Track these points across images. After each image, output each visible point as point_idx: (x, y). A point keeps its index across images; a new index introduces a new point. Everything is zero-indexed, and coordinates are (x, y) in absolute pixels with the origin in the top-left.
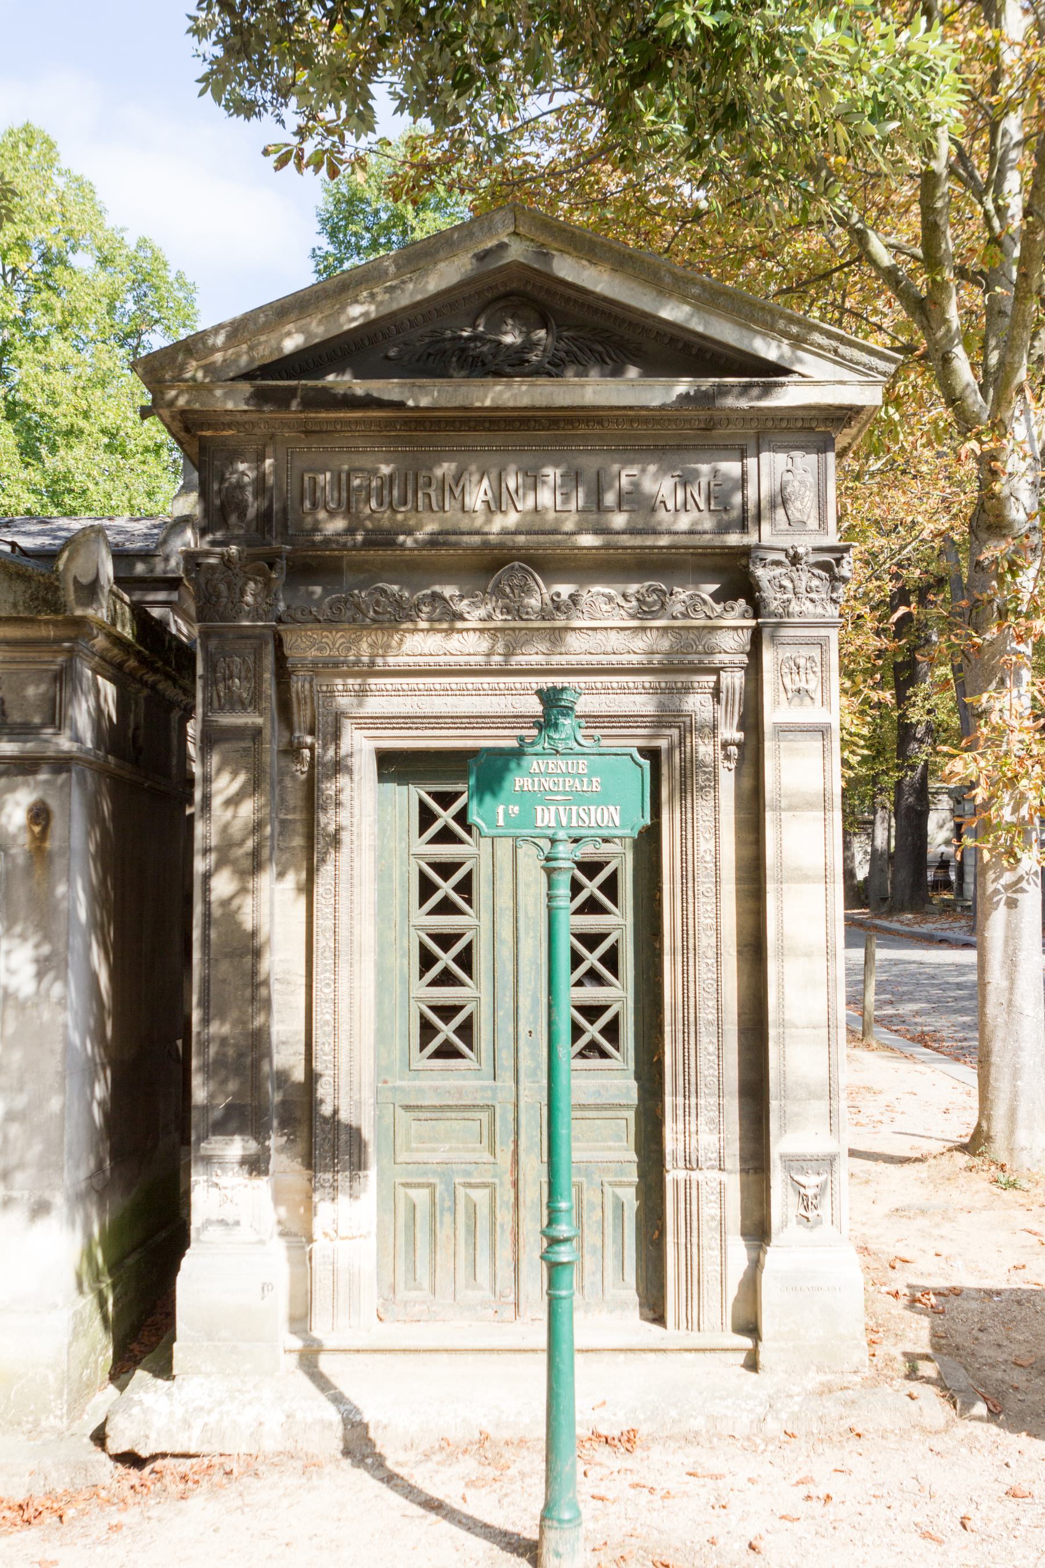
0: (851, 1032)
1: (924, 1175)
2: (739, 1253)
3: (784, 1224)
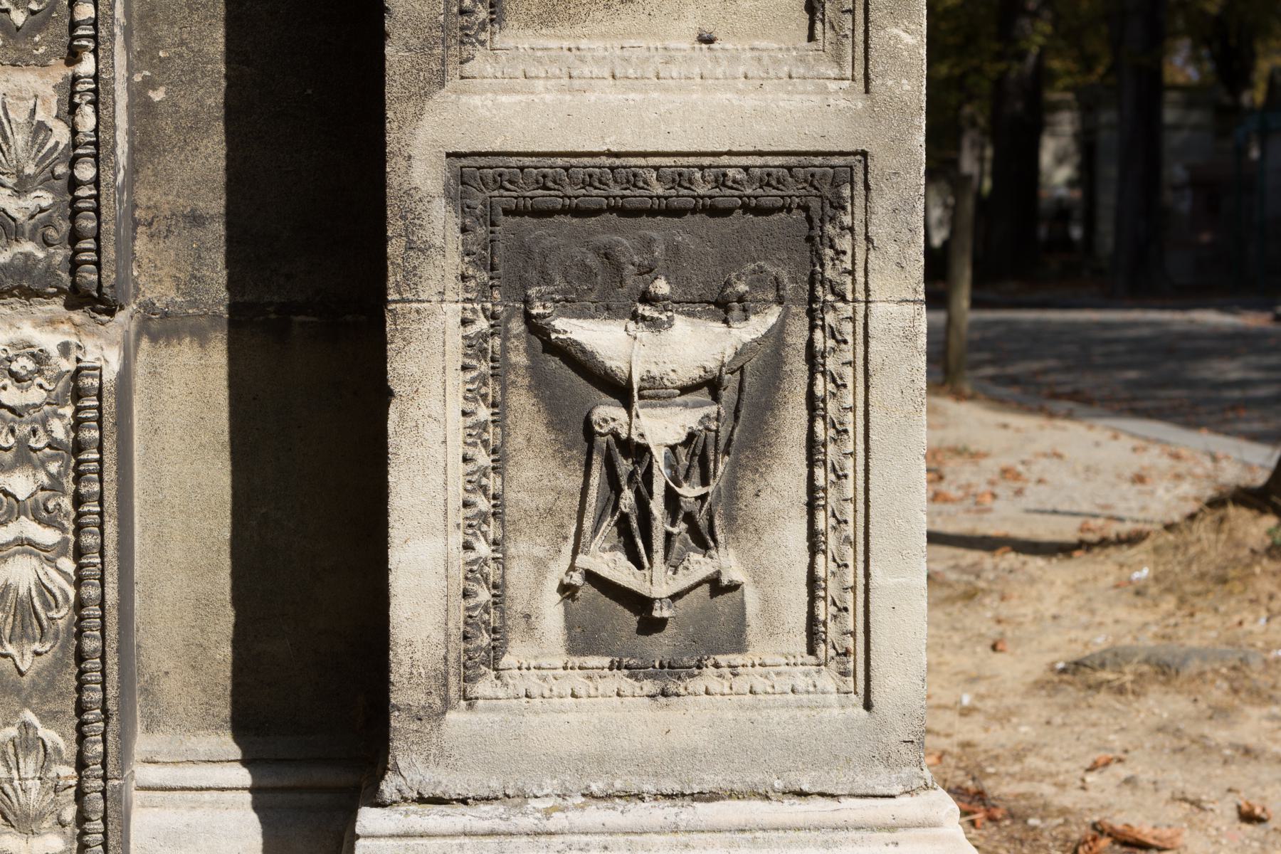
0: (944, 426)
3: (483, 641)
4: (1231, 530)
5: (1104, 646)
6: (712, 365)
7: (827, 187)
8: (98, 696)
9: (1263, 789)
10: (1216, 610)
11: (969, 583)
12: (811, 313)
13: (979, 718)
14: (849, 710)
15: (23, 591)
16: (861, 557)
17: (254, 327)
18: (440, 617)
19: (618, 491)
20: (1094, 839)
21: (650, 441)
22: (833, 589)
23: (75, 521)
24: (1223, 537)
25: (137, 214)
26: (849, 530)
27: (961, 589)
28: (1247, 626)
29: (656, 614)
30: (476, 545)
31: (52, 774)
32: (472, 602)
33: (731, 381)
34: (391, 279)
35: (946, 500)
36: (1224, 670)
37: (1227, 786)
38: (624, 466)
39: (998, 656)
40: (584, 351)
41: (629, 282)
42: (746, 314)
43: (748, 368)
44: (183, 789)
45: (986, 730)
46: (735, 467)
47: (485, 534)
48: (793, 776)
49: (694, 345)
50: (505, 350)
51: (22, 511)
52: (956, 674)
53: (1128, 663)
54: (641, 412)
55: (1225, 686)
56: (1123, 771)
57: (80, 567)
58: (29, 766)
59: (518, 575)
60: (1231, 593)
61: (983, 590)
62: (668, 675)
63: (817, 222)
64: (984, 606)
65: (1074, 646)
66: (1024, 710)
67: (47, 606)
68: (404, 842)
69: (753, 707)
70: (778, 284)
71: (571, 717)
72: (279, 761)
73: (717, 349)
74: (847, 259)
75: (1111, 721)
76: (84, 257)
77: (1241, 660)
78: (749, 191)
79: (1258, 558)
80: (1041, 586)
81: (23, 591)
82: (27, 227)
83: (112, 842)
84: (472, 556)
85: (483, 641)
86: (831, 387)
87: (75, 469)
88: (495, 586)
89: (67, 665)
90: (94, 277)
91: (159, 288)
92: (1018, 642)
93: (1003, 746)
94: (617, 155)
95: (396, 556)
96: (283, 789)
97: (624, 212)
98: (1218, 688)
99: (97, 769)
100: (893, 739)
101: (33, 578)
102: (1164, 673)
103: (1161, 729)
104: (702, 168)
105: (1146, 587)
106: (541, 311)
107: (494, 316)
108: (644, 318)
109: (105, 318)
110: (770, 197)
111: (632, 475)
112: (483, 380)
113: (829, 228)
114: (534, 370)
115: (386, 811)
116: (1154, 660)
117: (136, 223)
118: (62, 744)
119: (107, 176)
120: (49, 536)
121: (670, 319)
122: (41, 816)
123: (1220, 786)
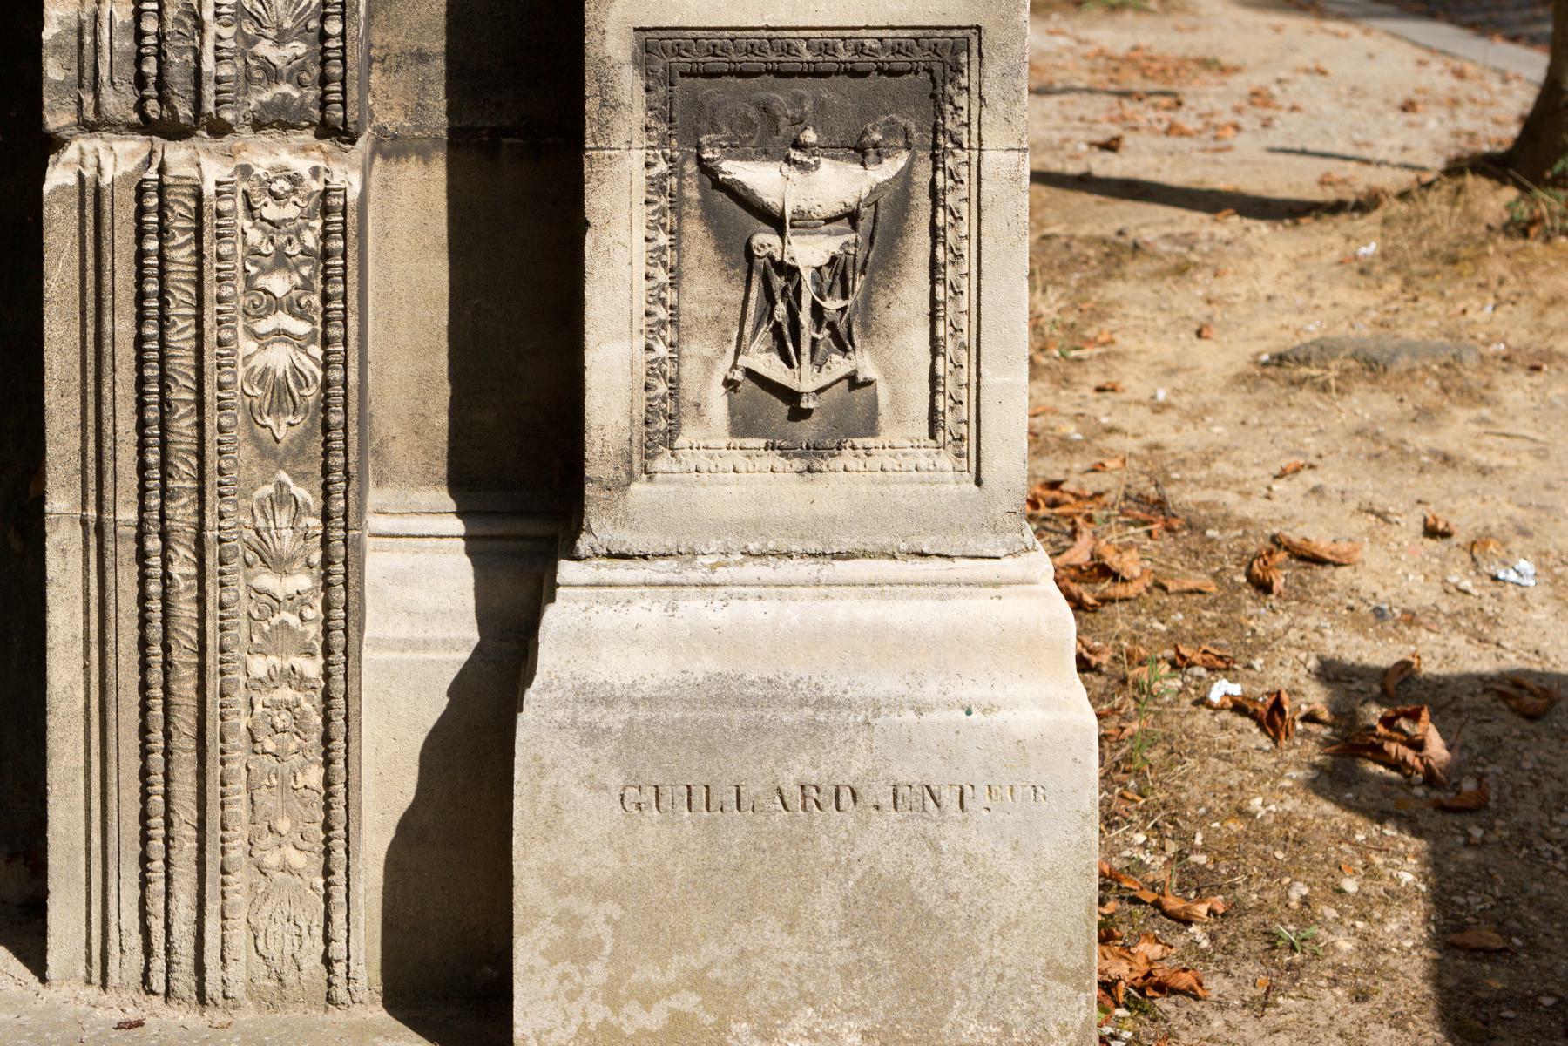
0: (1194, 29)
1: (1371, 249)
2: (422, 583)
3: (662, 426)
4: (1467, 202)
5: (1317, 336)
6: (851, 201)
7: (947, 54)
8: (341, 461)
9: (1454, 501)
10: (1442, 294)
11: (1180, 256)
12: (934, 157)
13: (1172, 416)
14: (963, 486)
15: (279, 373)
16: (974, 360)
17: (469, 148)
18: (627, 407)
19: (772, 303)
20: (1270, 553)
21: (799, 263)
22: (950, 386)
23: (323, 315)
24: (1458, 210)
25: (372, 52)
26: (964, 337)
27: (1172, 261)
28: (1471, 315)
29: (804, 405)
30: (656, 347)
31: (302, 525)
32: (652, 394)
33: (867, 213)
34: (588, 131)
35: (1183, 133)
36: (1435, 368)
37: (1417, 497)
38: (778, 282)
39: (1203, 343)
40: (745, 189)
41: (783, 131)
42: (880, 158)
43: (881, 202)
44: (408, 536)
45: (1178, 430)
46: (870, 283)
47: (663, 338)
48: (915, 540)
49: (836, 183)
50: (681, 186)
51: (279, 307)
52: (1155, 364)
53: (1333, 358)
54: (792, 239)
55: (1435, 384)
56: (1311, 479)
57: (326, 354)
58: (284, 518)
59: (691, 371)
60: (1460, 275)
61: (1195, 264)
62: (813, 455)
63: (939, 82)
64: (1195, 282)
65: (1285, 334)
66: (1221, 407)
67: (299, 385)
68: (596, 590)
69: (883, 482)
70: (906, 133)
71: (733, 488)
72: (488, 513)
73: (856, 187)
74: (964, 114)
75: (1310, 421)
76: (332, 97)
77: (1454, 356)
78: (883, 58)
79: (1493, 235)
80: (1259, 260)
81: (279, 373)
82: (285, 72)
83: (352, 582)
84: (653, 356)
85: (662, 426)
86: (950, 219)
87: (324, 272)
88: (671, 381)
89: (315, 435)
90: (340, 115)
91: (390, 115)
92: (1226, 327)
93: (1192, 449)
94: (774, 29)
95: (592, 357)
96: (491, 538)
97: (778, 74)
98: (1427, 386)
99: (339, 520)
100: (999, 510)
101: (288, 363)
102: (1371, 369)
103: (1359, 433)
104: (844, 39)
105: (1371, 264)
106: (710, 155)
107: (672, 160)
108: (795, 162)
109: (348, 146)
110: (901, 62)
111: (784, 290)
112: (663, 212)
113: (949, 87)
114: (705, 203)
115: (581, 564)
116: (1361, 355)
117: (371, 60)
118: (310, 500)
119: (351, 31)
120: (301, 328)
121: (817, 163)
122: (292, 559)
123: (1408, 495)
